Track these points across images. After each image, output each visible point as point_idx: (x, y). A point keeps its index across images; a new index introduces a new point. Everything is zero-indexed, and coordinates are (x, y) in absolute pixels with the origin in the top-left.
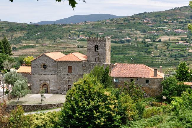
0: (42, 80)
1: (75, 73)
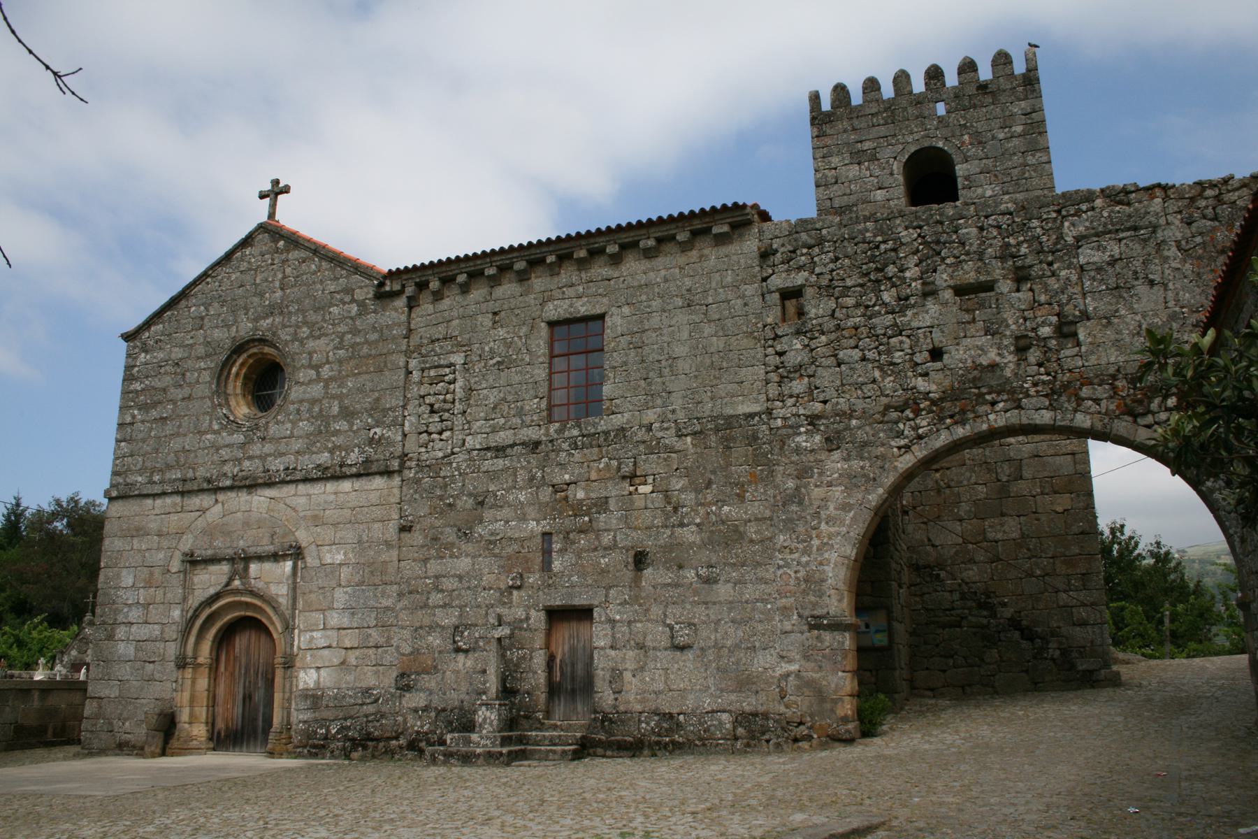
0: (214, 560)
1: (651, 416)
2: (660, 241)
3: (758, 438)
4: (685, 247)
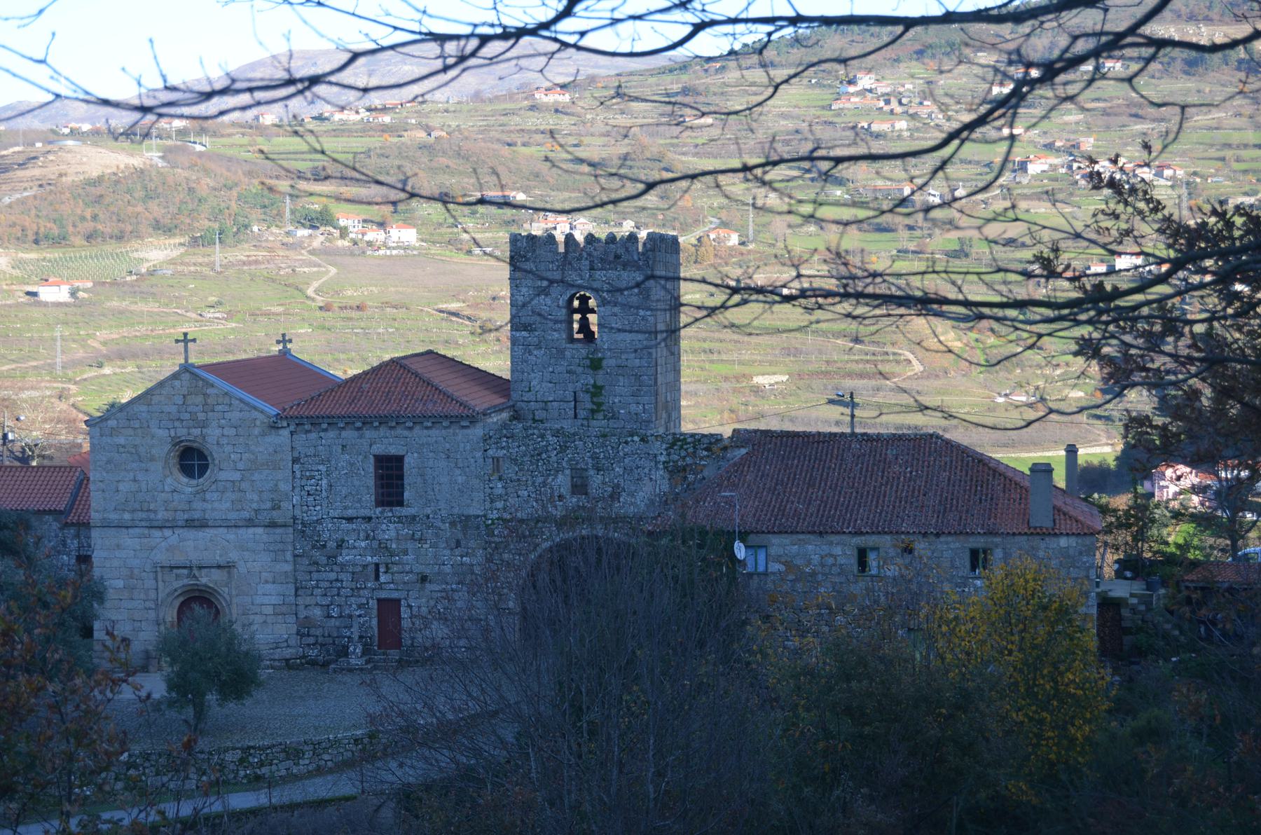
1: (428, 511)
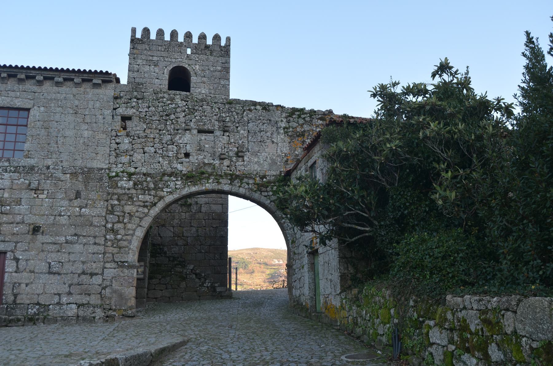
1: (49, 162)
2: (65, 80)
3: (103, 180)
4: (77, 85)
